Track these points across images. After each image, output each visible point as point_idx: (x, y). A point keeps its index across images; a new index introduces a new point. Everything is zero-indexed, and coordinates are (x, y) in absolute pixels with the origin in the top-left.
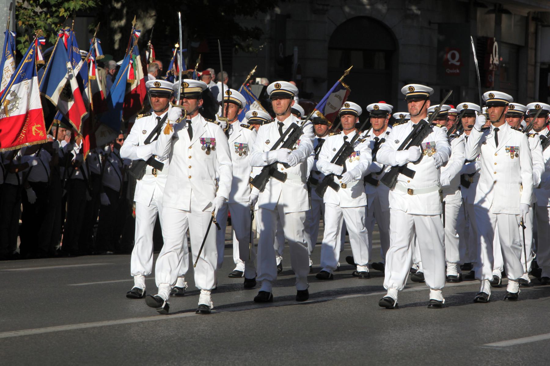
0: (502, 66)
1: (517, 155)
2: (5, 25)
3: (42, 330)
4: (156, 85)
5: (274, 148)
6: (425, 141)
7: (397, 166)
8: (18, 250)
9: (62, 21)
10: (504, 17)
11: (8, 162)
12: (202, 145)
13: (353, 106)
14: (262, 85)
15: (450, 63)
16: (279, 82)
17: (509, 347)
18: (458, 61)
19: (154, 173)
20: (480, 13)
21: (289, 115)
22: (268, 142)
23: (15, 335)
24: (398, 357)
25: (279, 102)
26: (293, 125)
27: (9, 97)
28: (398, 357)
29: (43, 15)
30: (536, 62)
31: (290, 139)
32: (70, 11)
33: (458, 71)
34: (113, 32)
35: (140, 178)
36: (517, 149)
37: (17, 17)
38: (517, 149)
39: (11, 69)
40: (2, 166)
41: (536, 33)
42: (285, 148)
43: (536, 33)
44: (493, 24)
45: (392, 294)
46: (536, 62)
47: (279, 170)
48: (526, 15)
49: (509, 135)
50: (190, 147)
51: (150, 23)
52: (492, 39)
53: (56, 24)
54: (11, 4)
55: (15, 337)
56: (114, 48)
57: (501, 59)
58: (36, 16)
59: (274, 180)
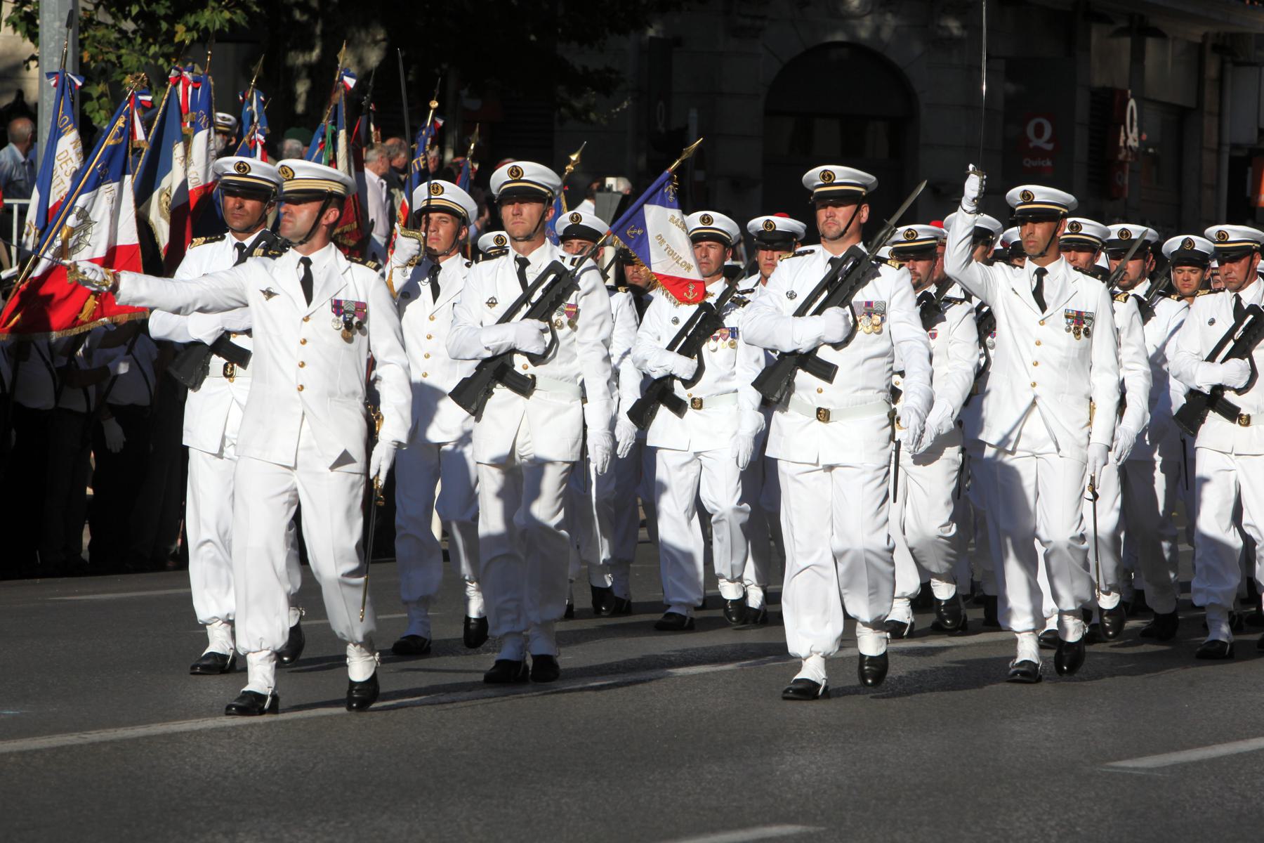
0: (1146, 153)
1: (1088, 333)
2: (56, 60)
3: (140, 731)
4: (238, 168)
5: (507, 318)
6: (861, 297)
7: (794, 352)
8: (85, 555)
9: (180, 53)
10: (1151, 44)
11: (64, 361)
13: (720, 220)
14: (618, 192)
15: (1031, 145)
16: (520, 164)
17: (1162, 769)
18: (1048, 142)
19: (228, 374)
20: (1097, 35)
22: (492, 303)
23: (81, 741)
24: (919, 792)
26: (554, 267)
27: (71, 221)
28: (919, 792)
29: (139, 40)
30: (1220, 144)
31: (550, 298)
32: (198, 31)
33: (1049, 163)
34: (291, 75)
35: (196, 385)
36: (1091, 318)
37: (82, 44)
38: (1091, 318)
39: (74, 157)
40: (50, 370)
41: (1221, 80)
43: (1221, 80)
44: (1126, 59)
46: (1220, 144)
47: (518, 368)
48: (1199, 40)
49: (1074, 287)
50: (306, 319)
51: (374, 58)
52: (1124, 93)
53: (167, 57)
54: (71, 14)
55: (81, 746)
56: (294, 111)
57: (1144, 136)
58: (125, 41)
59: (501, 393)
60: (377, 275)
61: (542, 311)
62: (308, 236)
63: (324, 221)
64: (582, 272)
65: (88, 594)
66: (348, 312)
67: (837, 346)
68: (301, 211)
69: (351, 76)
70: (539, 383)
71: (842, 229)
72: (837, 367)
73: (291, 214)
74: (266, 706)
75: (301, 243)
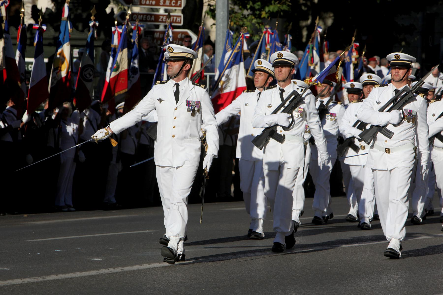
4: (396, 57)
5: (275, 112)
6: (407, 107)
7: (378, 126)
8: (232, 194)
9: (263, 22)
12: (187, 107)
14: (415, 68)
22: (270, 106)
25: (281, 70)
26: (294, 93)
31: (292, 104)
34: (300, 29)
35: (252, 135)
45: (394, 244)
47: (278, 132)
50: (176, 109)
51: (330, 22)
59: (272, 142)
61: (289, 110)
62: (177, 75)
63: (184, 69)
65: (233, 208)
66: (193, 105)
68: (176, 65)
69: (320, 28)
71: (401, 78)
73: (172, 66)
74: (180, 258)
75: (175, 77)
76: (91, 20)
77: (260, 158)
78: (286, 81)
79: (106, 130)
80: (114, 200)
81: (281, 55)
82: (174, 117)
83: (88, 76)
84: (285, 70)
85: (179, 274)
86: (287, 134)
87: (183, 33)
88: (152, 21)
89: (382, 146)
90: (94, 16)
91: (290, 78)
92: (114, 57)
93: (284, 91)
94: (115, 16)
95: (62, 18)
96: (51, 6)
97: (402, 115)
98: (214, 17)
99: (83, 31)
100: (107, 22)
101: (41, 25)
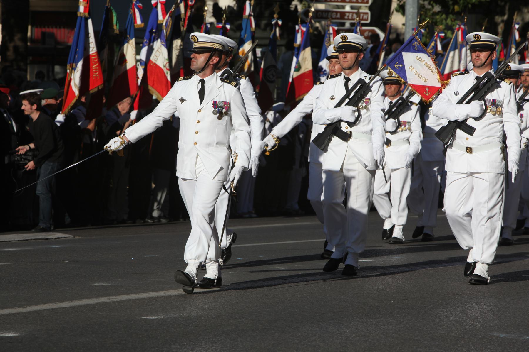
4: (475, 37)
5: (339, 105)
6: (490, 97)
7: (456, 121)
12: (213, 109)
21: (357, 70)
22: (332, 98)
26: (361, 81)
42: (349, 105)
50: (200, 111)
59: (335, 140)
60: (236, 89)
62: (203, 69)
64: (374, 83)
66: (220, 107)
67: (476, 119)
68: (201, 57)
70: (353, 135)
71: (483, 62)
72: (475, 129)
73: (196, 58)
75: (200, 72)
76: (273, 18)
77: (241, 169)
78: (351, 68)
79: (122, 138)
80: (297, 207)
81: (345, 37)
82: (197, 120)
83: (271, 77)
84: (351, 56)
85: (202, 305)
86: (353, 129)
87: (370, 31)
88: (338, 19)
89: (463, 145)
90: (278, 14)
91: (357, 64)
92: (297, 57)
93: (350, 80)
94: (298, 14)
95: (244, 16)
96: (232, 3)
97: (484, 106)
98: (404, 14)
99: (265, 30)
100: (291, 19)
101: (225, 24)
